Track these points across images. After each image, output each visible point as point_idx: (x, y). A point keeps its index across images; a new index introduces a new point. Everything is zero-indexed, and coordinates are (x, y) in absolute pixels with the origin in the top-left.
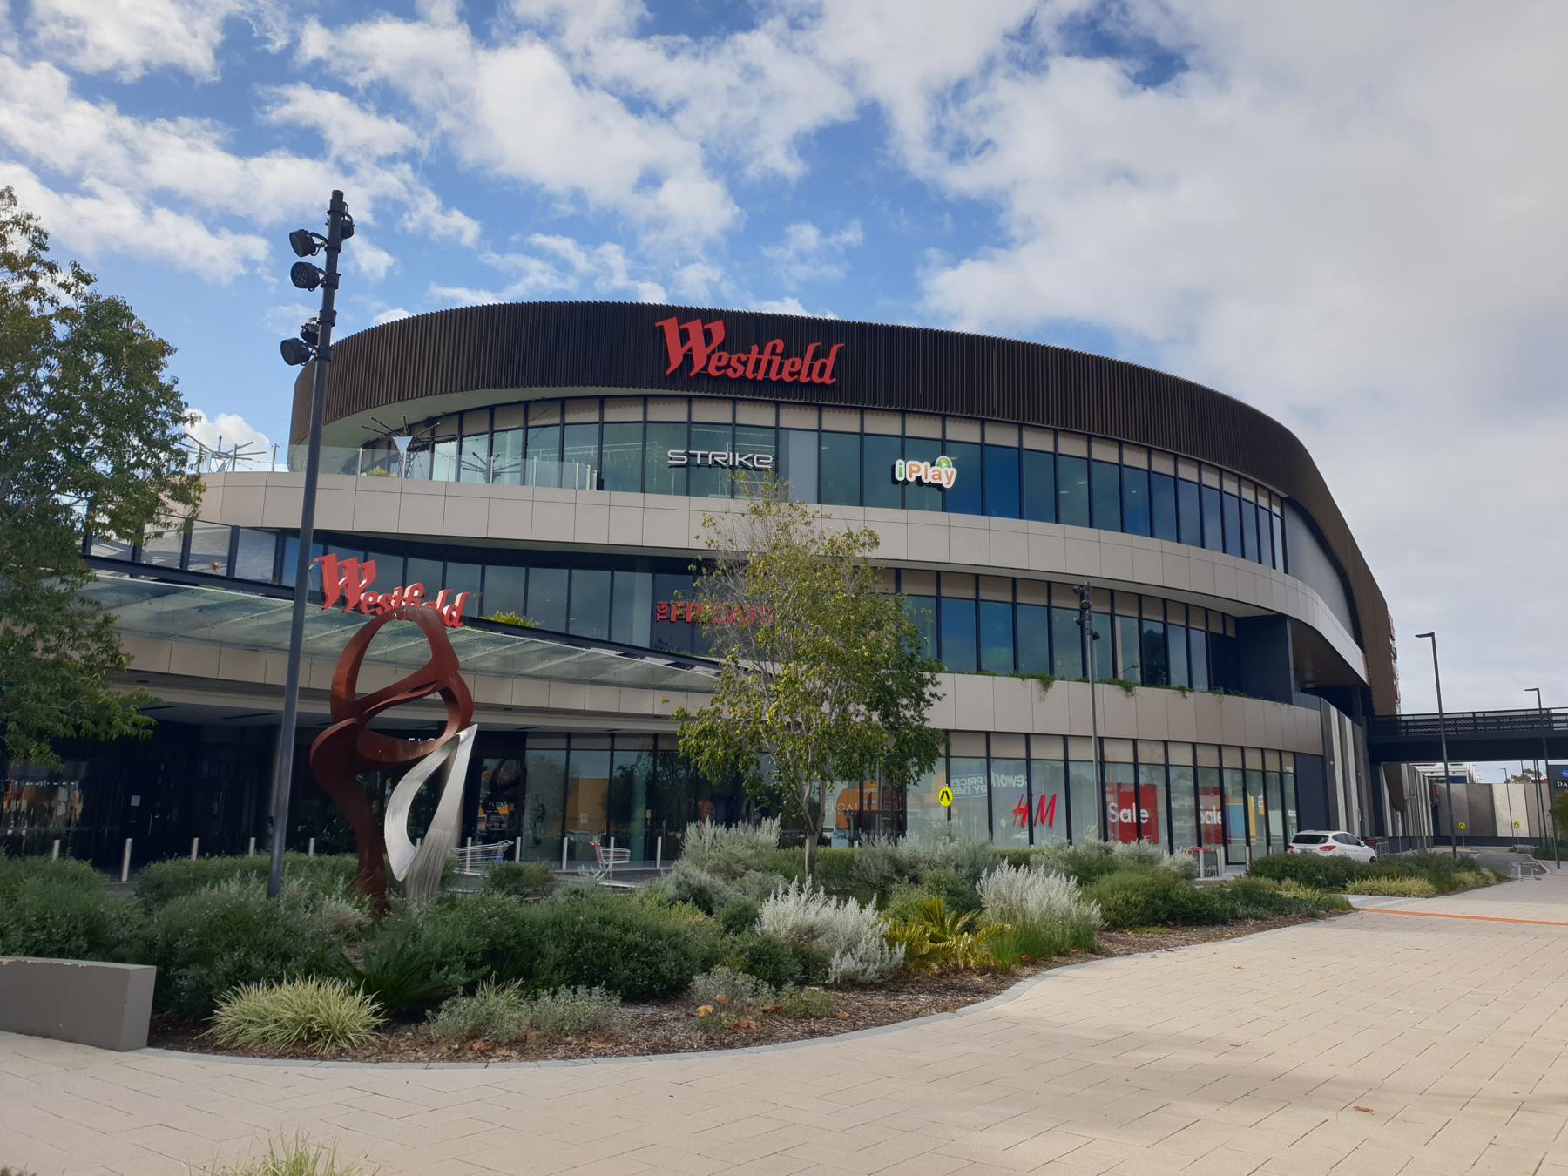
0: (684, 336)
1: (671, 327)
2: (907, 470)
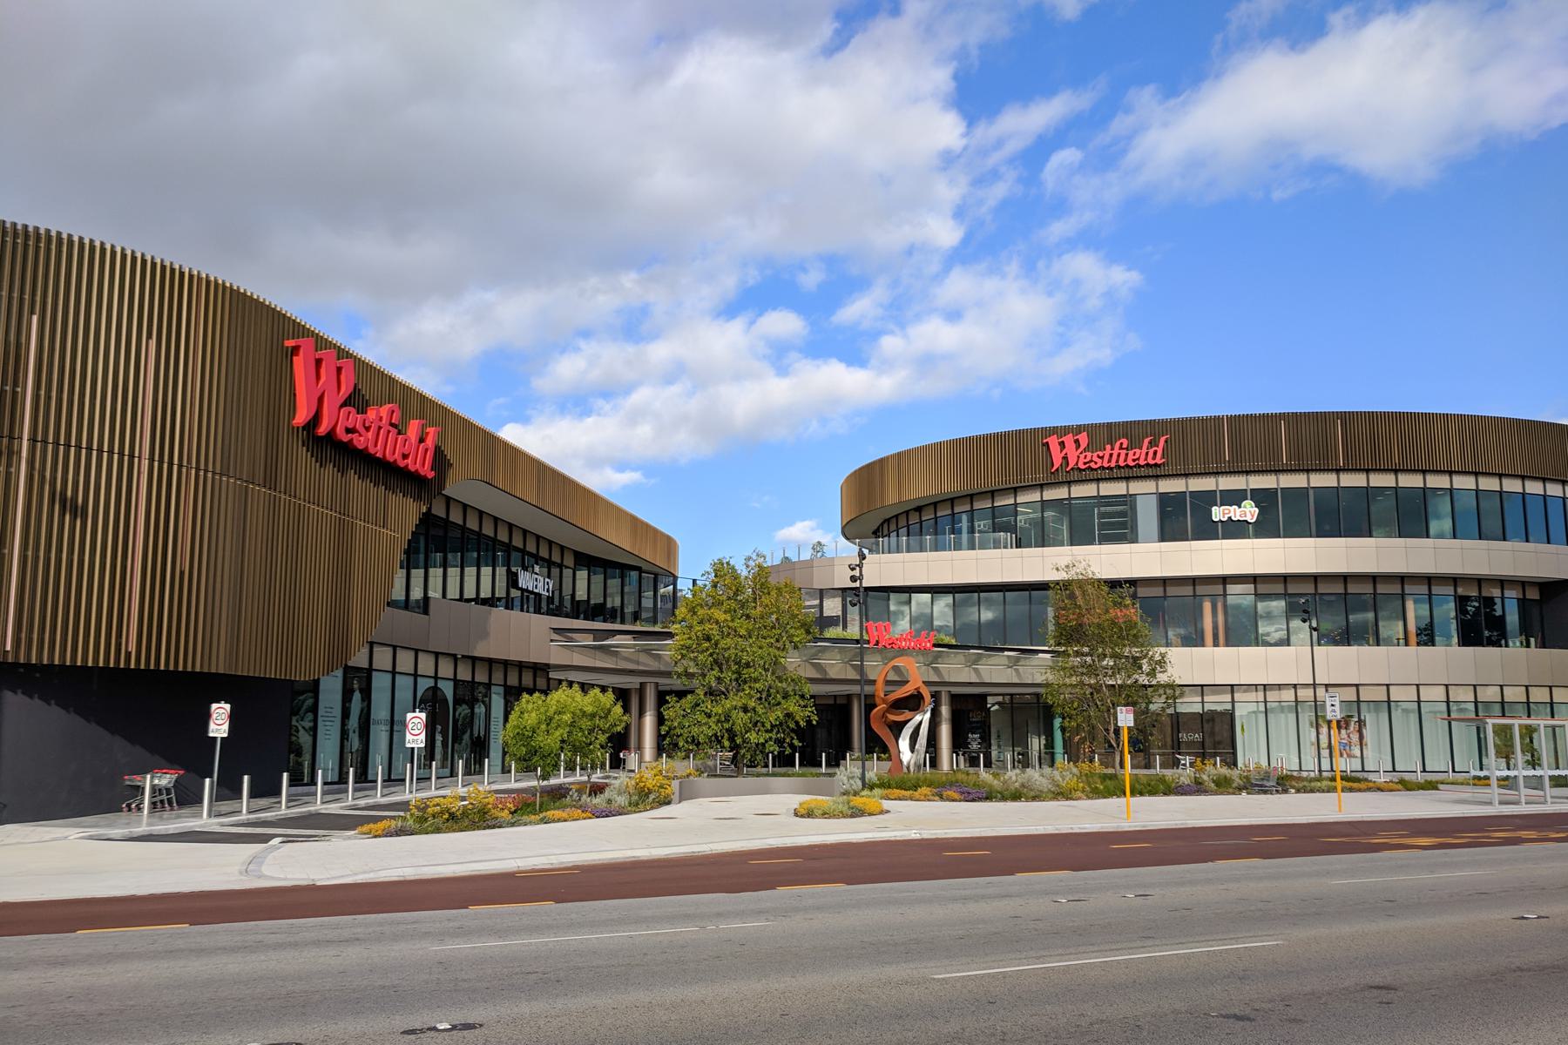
0: (1062, 444)
1: (1053, 442)
2: (1219, 513)
